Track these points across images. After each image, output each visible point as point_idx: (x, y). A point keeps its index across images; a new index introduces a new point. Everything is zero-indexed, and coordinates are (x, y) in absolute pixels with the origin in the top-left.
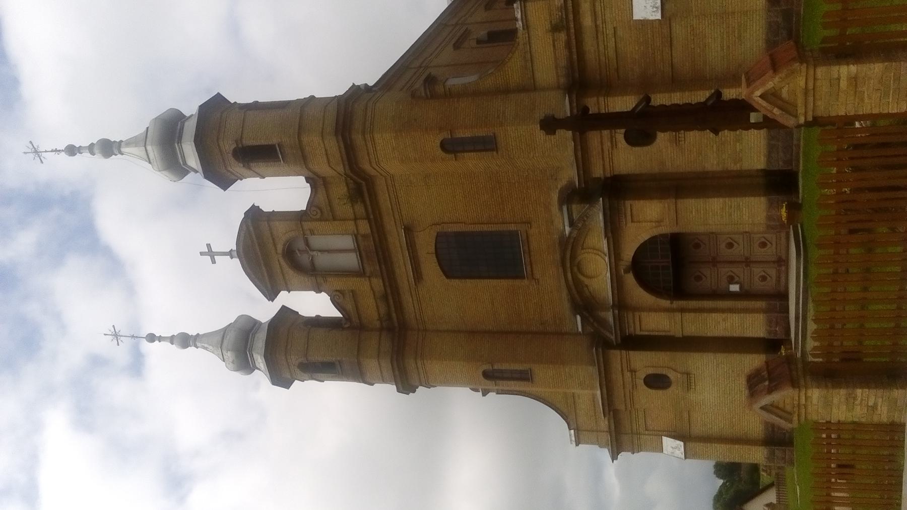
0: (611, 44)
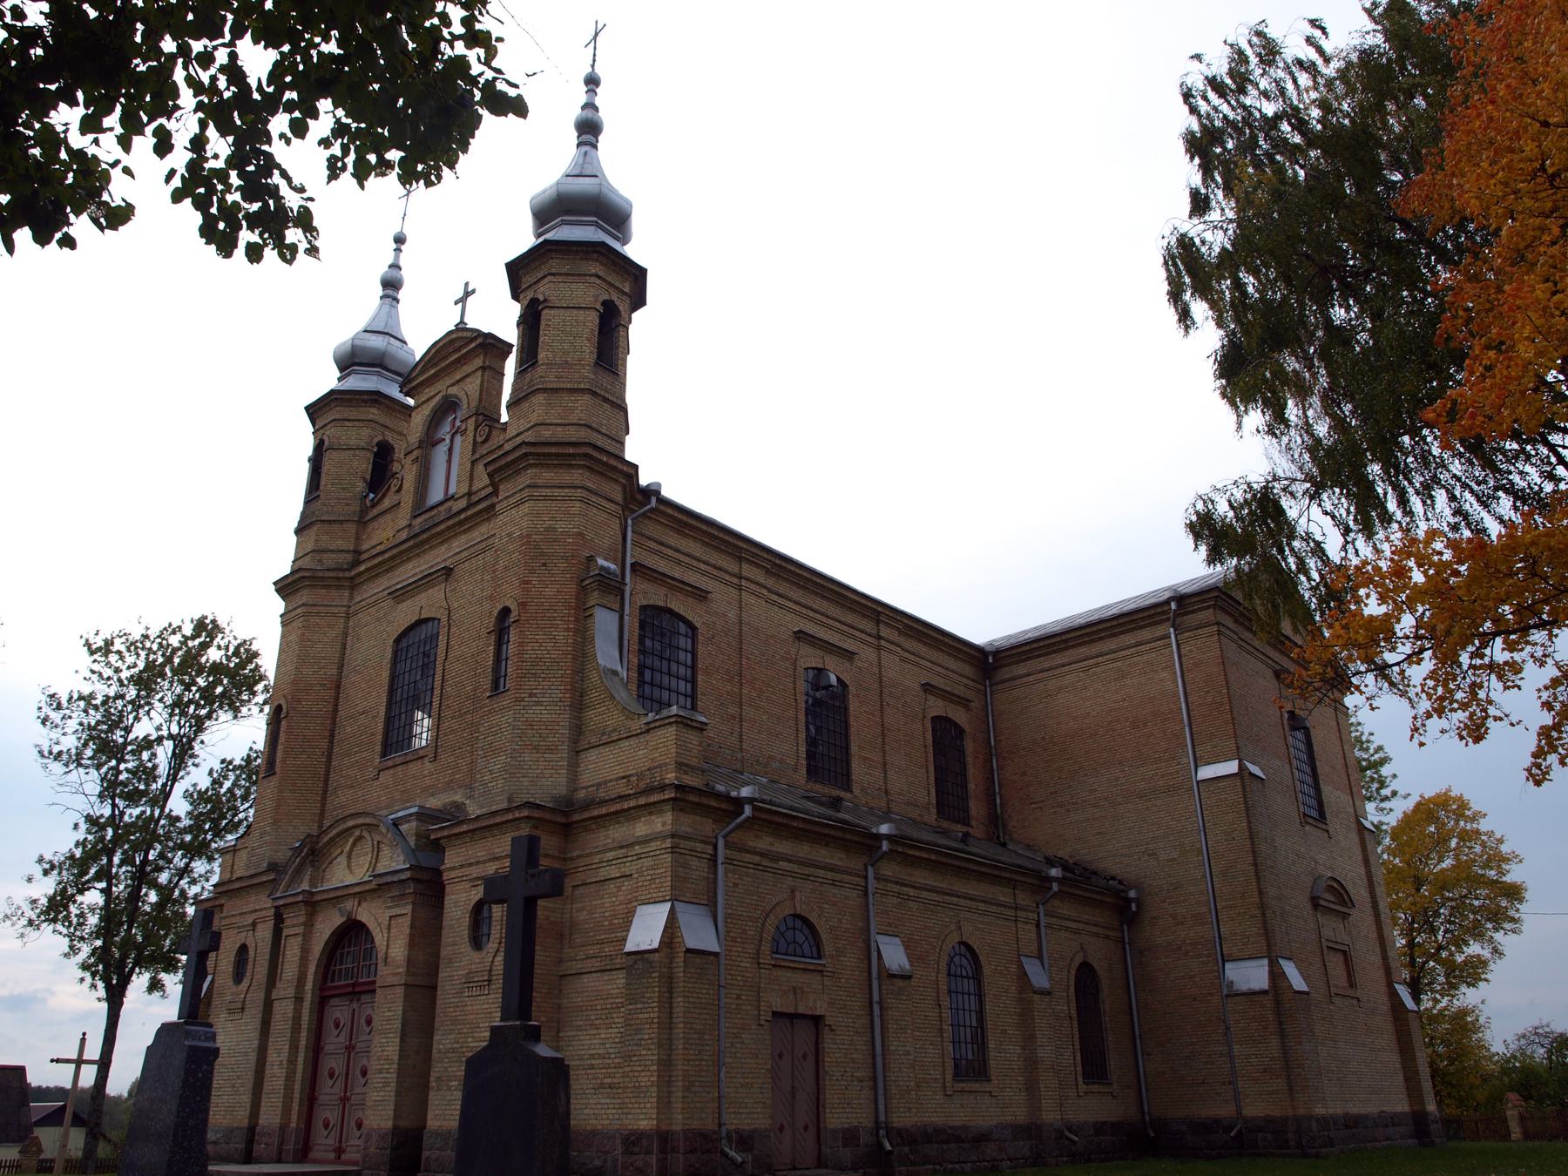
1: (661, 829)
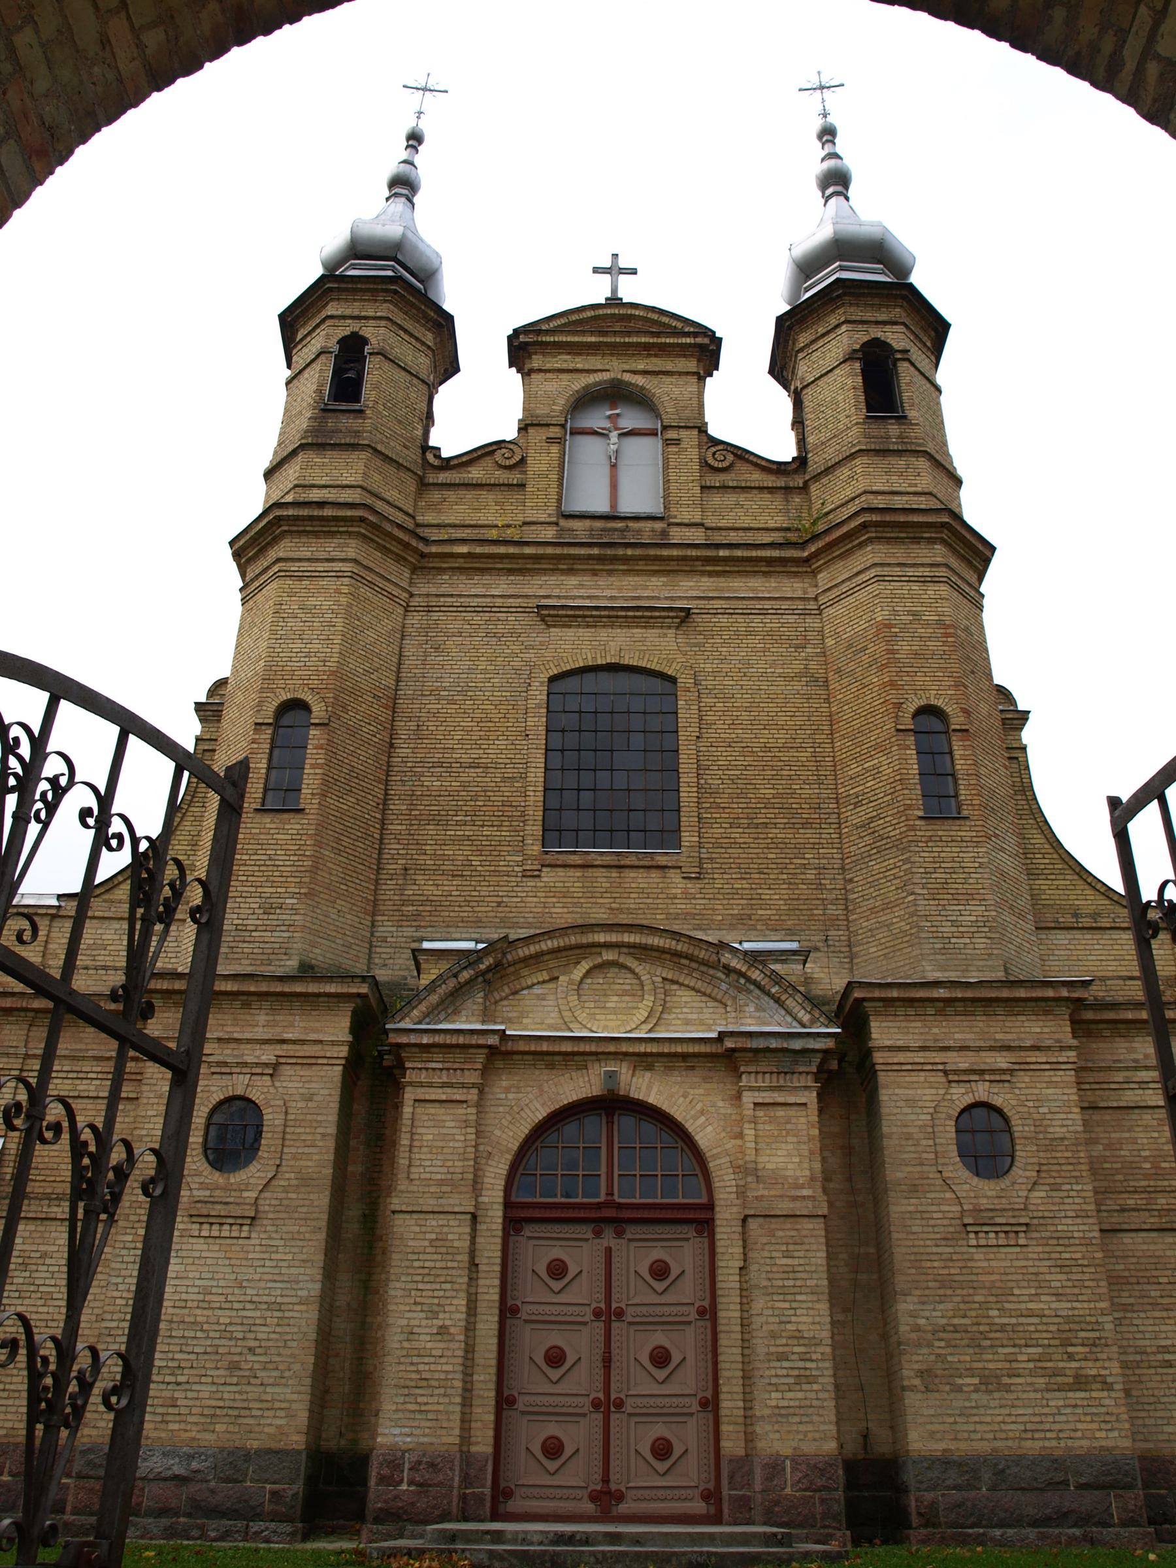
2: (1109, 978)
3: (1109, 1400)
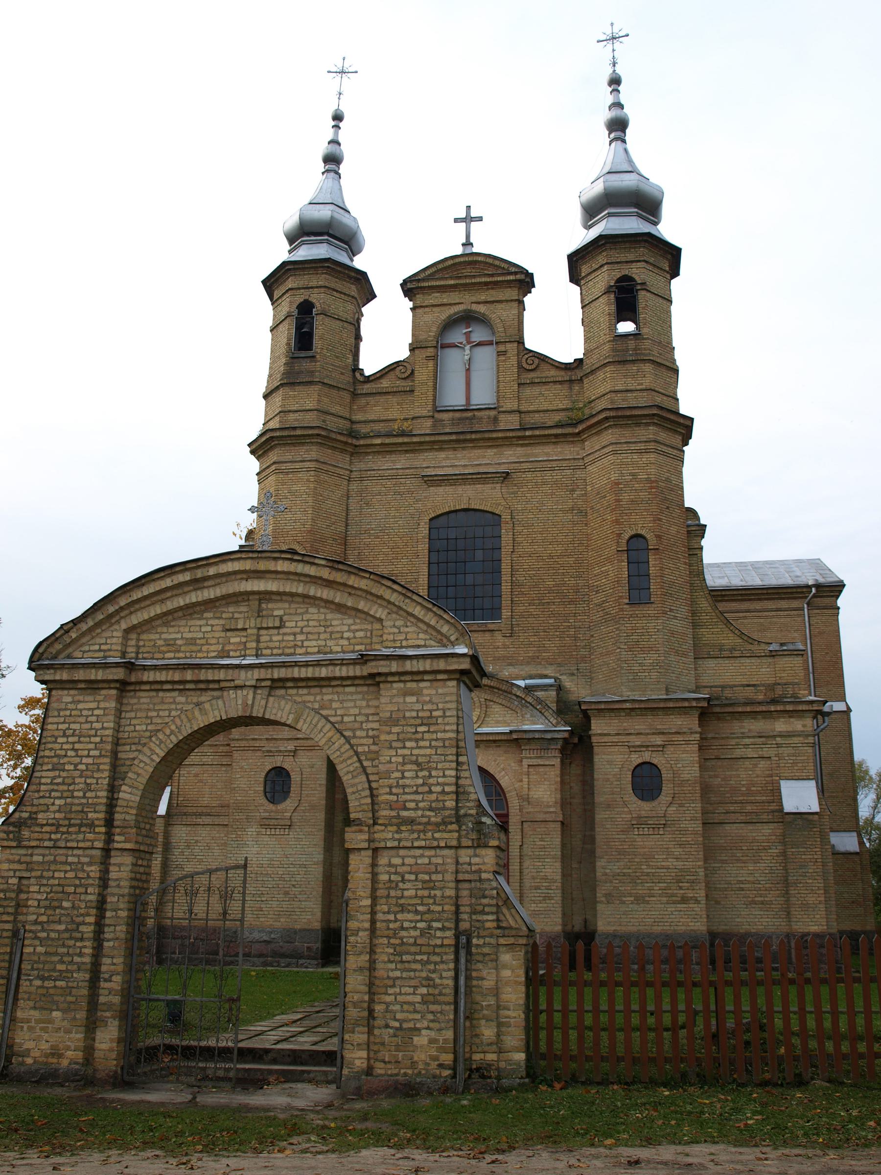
0: (750, 753)
1: (802, 729)
2: (735, 686)
3: (697, 908)
